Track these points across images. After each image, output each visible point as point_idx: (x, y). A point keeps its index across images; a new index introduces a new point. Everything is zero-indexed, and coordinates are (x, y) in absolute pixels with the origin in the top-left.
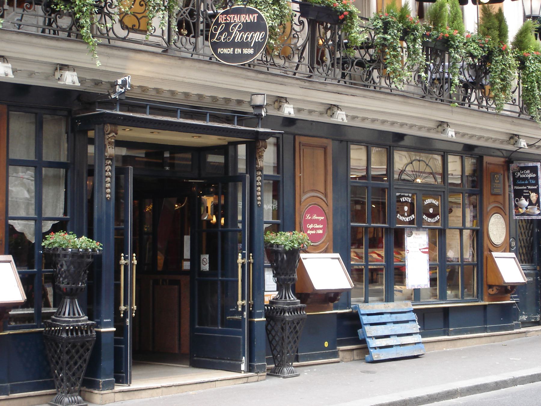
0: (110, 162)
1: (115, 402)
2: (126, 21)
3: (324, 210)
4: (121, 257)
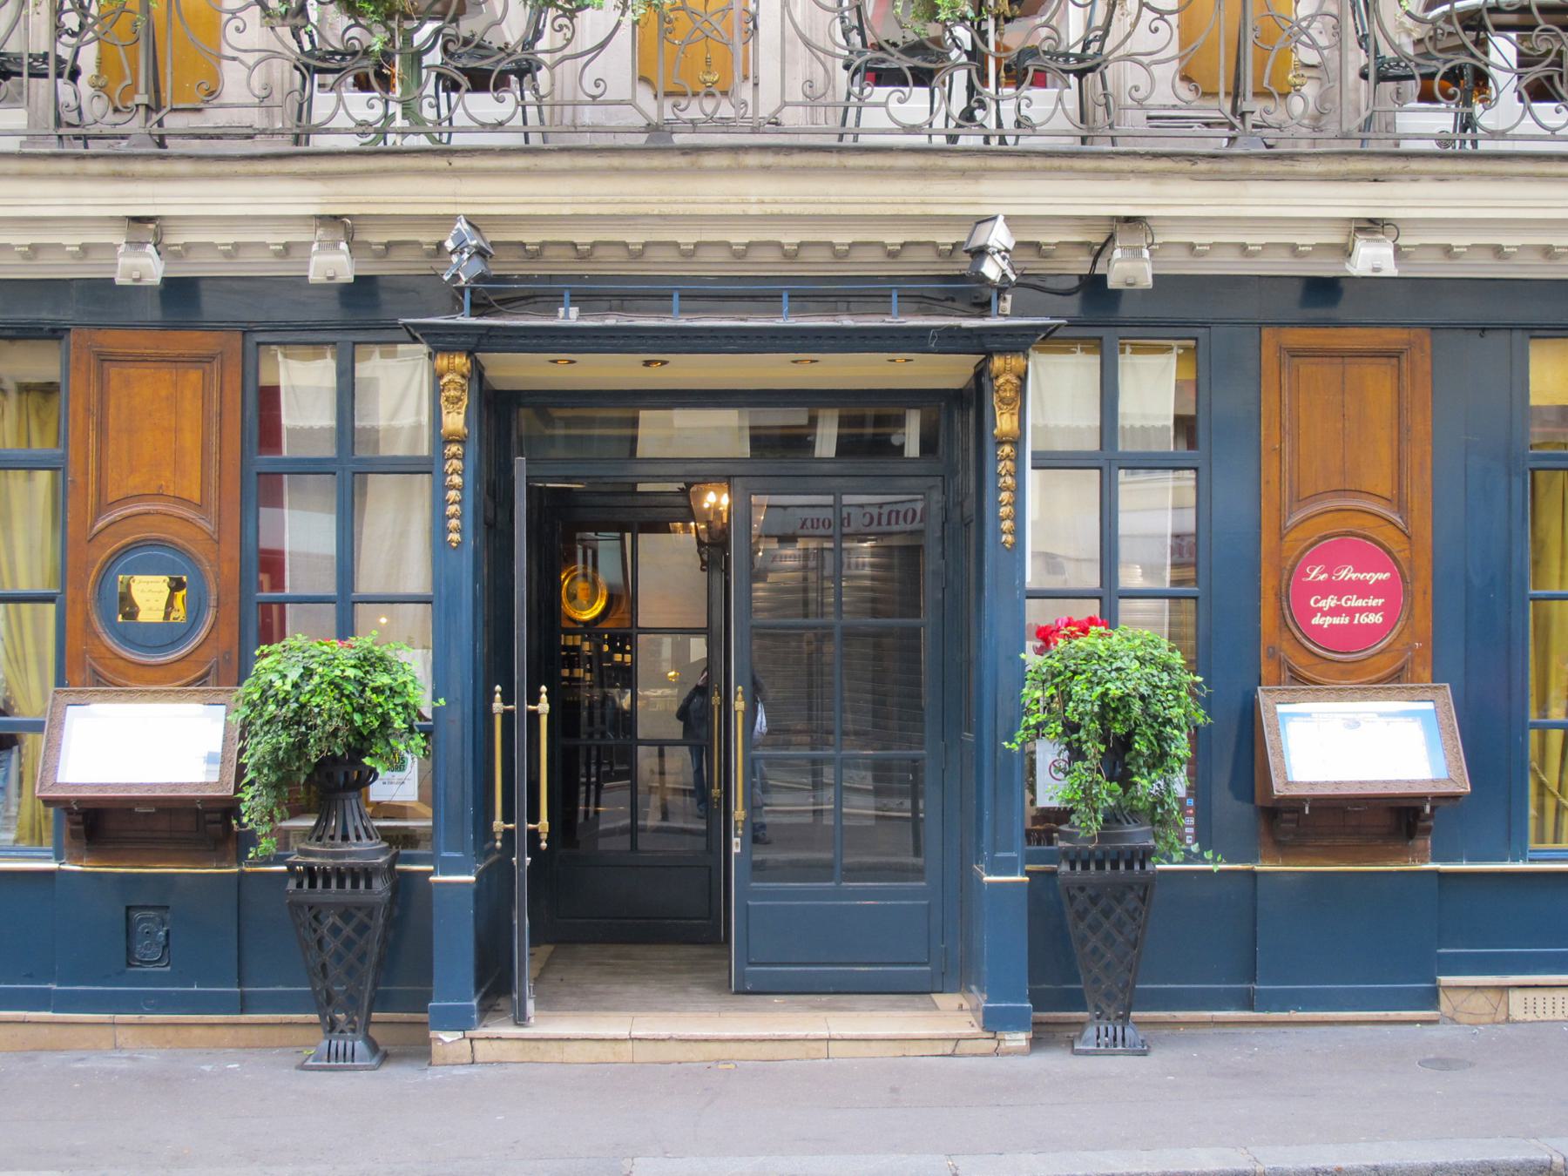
0: (454, 448)
1: (473, 1063)
2: (451, 47)
3: (1389, 553)
4: (495, 693)
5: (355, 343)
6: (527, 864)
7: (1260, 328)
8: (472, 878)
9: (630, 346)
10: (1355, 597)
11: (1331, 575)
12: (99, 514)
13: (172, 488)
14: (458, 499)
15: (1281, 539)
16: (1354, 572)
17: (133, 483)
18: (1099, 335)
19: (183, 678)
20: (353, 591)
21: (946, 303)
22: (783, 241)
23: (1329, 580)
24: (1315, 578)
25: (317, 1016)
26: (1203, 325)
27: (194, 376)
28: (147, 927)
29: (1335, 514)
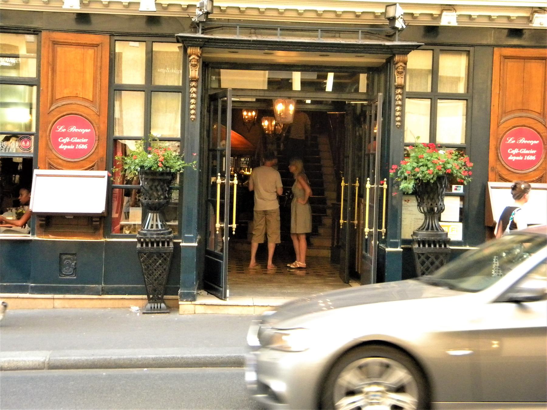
0: (194, 84)
5: (116, 40)
6: (228, 240)
7: (493, 48)
8: (196, 244)
9: (261, 47)
10: (76, 138)
11: (67, 129)
12: (52, 104)
13: (81, 94)
14: (194, 103)
15: (498, 127)
16: (525, 140)
17: (66, 92)
18: (468, 50)
19: (85, 167)
20: (113, 135)
21: (376, 35)
22: (318, 10)
23: (515, 143)
24: (61, 130)
25: (146, 296)
26: (472, 46)
27: (91, 51)
28: (67, 262)
29: (519, 118)
